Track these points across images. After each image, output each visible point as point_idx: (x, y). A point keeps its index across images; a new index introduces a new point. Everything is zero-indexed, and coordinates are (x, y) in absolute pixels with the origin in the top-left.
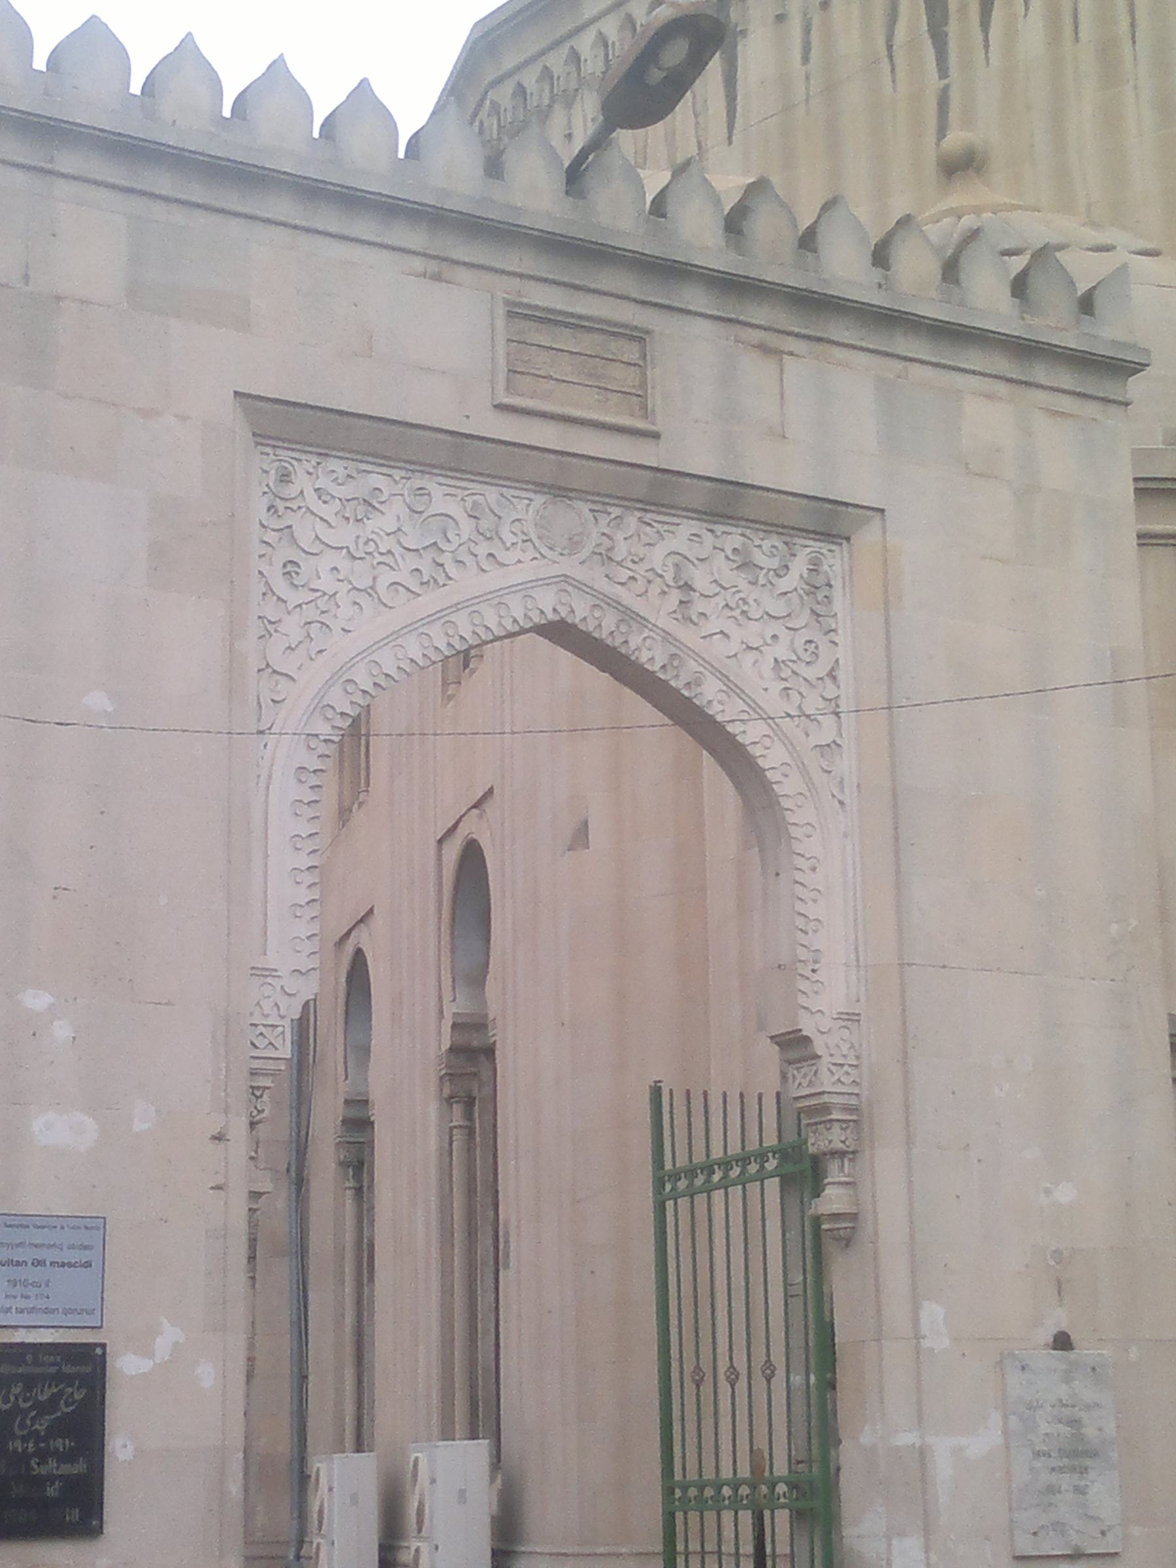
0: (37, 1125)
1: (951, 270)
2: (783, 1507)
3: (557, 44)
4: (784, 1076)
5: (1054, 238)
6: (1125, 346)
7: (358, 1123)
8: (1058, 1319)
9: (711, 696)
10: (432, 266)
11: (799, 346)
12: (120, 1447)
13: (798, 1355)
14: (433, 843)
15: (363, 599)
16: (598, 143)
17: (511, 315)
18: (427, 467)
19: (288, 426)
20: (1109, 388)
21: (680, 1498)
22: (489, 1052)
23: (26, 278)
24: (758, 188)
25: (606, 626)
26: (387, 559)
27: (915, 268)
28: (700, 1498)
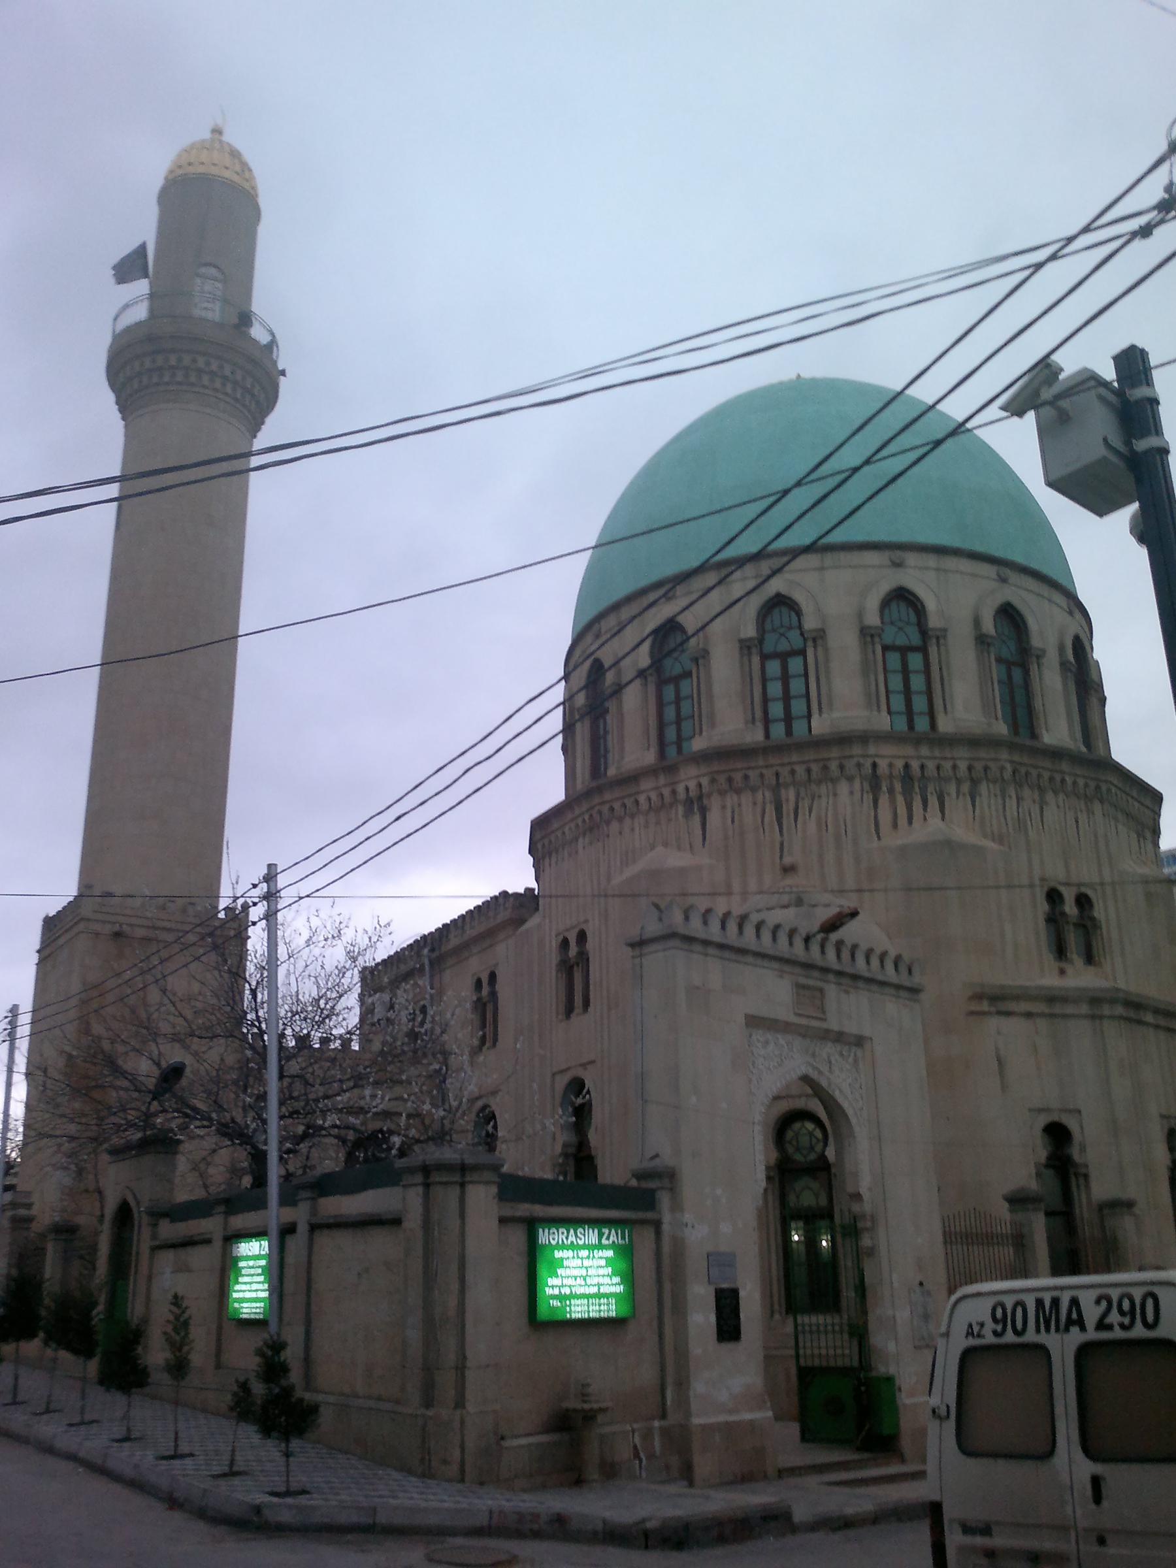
19: (754, 1022)
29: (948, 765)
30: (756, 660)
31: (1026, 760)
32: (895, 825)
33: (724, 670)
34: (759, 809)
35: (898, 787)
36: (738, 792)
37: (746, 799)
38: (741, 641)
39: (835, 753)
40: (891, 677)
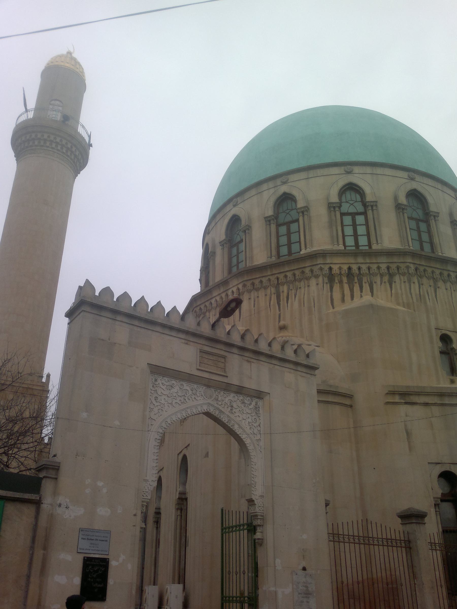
0: (98, 510)
1: (283, 348)
2: (246, 603)
3: (207, 301)
4: (248, 508)
5: (300, 343)
6: (315, 364)
7: (158, 513)
8: (303, 564)
9: (236, 428)
10: (186, 342)
11: (255, 361)
12: (111, 581)
13: (250, 569)
14: (176, 456)
15: (170, 405)
16: (218, 320)
17: (200, 352)
18: (183, 380)
19: (157, 370)
20: (312, 372)
21: (225, 600)
22: (186, 499)
23: (109, 339)
24: (247, 331)
25: (216, 413)
26: (175, 398)
27: (276, 347)
28: (236, 600)
29: (374, 267)
30: (273, 227)
31: (423, 263)
32: (343, 300)
33: (258, 234)
34: (268, 297)
35: (345, 280)
36: (257, 290)
37: (261, 293)
38: (265, 218)
39: (308, 264)
40: (346, 229)
